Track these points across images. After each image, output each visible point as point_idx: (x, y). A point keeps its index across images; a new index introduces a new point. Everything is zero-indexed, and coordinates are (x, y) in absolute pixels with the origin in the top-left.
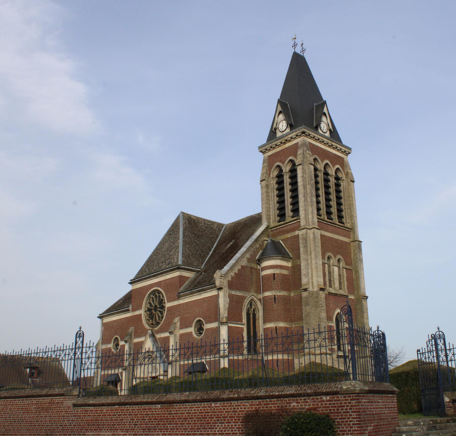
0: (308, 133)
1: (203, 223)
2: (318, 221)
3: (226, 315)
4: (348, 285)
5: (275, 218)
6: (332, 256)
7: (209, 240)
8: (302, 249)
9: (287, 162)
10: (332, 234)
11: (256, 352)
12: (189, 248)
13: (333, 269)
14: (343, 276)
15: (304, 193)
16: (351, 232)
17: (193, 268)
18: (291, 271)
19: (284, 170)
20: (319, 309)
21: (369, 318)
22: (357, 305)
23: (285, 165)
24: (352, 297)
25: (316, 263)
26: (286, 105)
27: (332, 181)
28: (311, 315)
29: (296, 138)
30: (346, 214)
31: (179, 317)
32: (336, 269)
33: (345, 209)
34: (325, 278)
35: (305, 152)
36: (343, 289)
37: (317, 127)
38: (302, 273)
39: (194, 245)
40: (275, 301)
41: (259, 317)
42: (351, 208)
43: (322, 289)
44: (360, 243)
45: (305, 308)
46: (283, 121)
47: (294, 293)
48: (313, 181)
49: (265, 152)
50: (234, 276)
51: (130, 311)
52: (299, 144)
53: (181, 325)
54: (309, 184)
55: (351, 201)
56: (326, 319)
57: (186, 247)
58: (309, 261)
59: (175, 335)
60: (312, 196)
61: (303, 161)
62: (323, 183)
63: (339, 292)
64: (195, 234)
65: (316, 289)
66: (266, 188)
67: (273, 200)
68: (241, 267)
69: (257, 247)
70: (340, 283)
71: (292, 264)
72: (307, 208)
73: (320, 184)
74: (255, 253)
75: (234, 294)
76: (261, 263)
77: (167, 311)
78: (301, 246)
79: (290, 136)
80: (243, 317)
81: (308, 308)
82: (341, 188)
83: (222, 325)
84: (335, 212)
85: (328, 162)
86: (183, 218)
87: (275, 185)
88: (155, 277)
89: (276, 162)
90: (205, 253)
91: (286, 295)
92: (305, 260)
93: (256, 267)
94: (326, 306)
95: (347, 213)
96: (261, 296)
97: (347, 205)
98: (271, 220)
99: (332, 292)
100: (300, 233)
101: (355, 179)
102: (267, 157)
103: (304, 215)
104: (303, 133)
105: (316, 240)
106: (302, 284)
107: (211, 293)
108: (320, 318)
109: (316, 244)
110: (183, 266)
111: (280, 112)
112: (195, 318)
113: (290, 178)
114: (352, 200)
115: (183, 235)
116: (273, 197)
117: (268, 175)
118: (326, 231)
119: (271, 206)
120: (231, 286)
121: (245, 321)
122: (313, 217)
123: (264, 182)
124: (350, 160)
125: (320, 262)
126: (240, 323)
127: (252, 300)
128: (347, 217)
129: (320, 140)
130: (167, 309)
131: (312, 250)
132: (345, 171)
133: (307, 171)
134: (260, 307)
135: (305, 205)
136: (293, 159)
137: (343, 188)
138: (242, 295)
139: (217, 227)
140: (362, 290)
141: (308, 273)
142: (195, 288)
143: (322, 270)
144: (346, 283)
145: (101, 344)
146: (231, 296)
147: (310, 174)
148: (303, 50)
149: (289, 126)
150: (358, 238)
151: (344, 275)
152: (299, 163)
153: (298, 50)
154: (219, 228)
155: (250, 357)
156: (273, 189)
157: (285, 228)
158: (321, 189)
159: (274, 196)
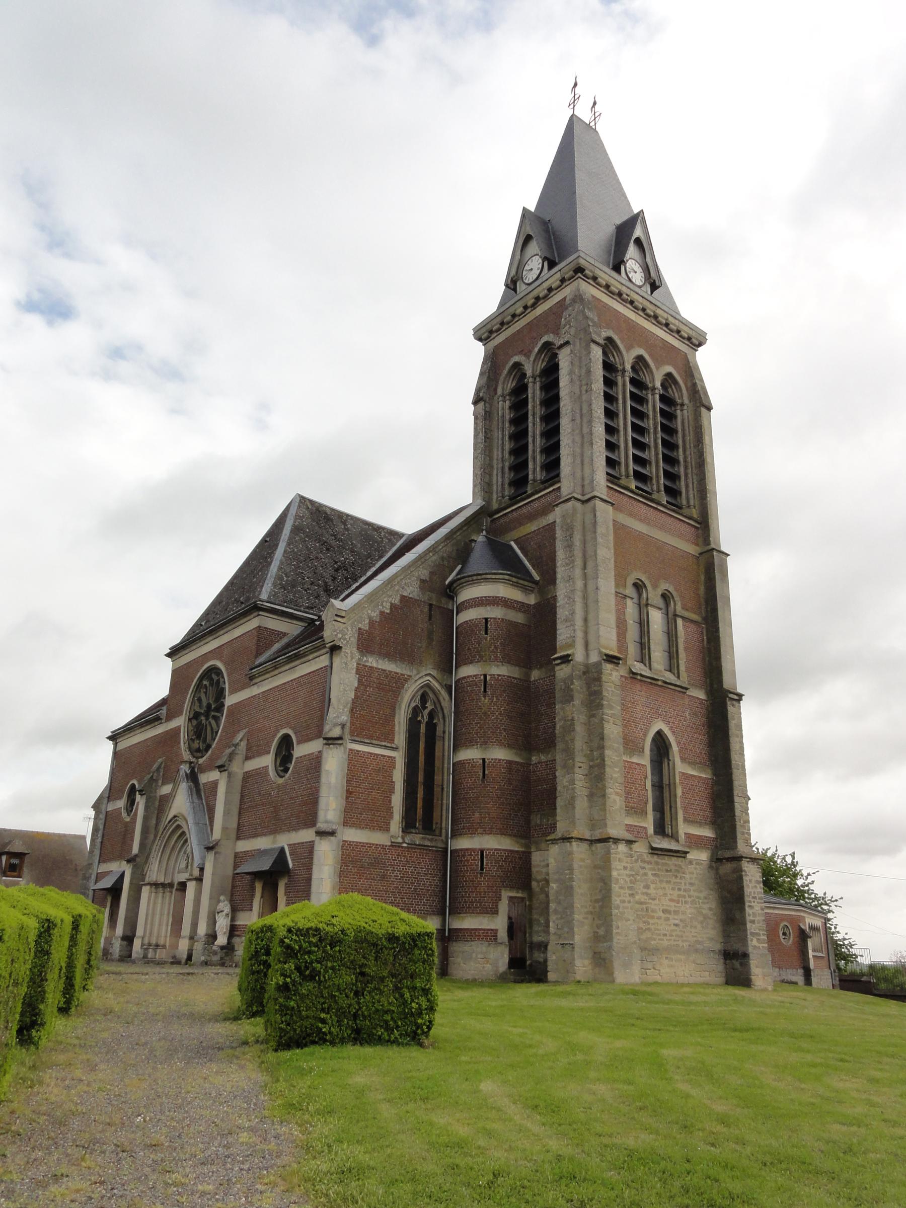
2: (608, 486)
8: (560, 555)
27: (654, 404)
38: (558, 616)
40: (485, 691)
41: (444, 732)
43: (612, 659)
51: (161, 719)
53: (249, 748)
68: (401, 601)
75: (375, 665)
83: (329, 744)
89: (512, 357)
91: (516, 676)
103: (570, 468)
106: (558, 644)
120: (366, 644)
121: (400, 737)
123: (481, 404)
124: (703, 358)
136: (550, 340)
138: (398, 670)
145: (105, 801)
146: (364, 674)
153: (584, 114)
157: (525, 510)
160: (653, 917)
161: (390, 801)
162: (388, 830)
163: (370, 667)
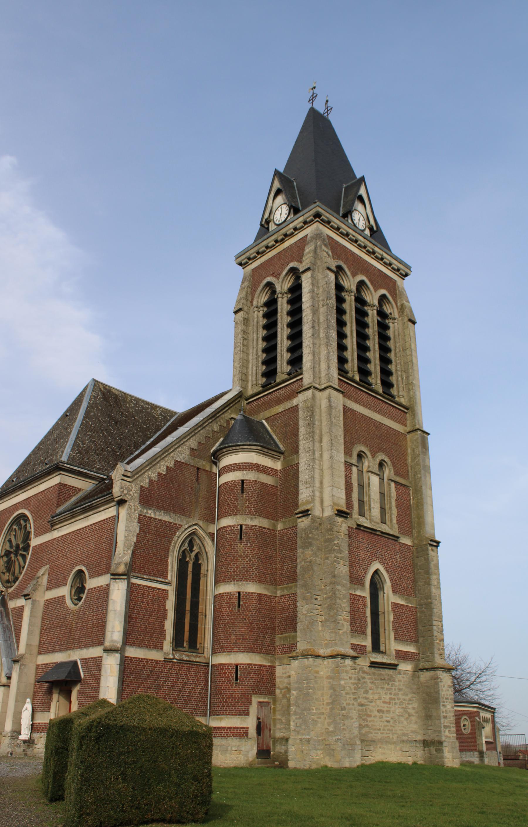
0: (326, 217)
1: (134, 404)
2: (339, 379)
3: (127, 558)
4: (399, 516)
5: (257, 380)
6: (368, 453)
7: (140, 431)
8: (302, 431)
9: (284, 273)
10: (369, 411)
11: (193, 644)
12: (91, 437)
13: (369, 479)
14: (390, 496)
15: (314, 321)
16: (407, 415)
17: (89, 472)
18: (281, 479)
19: (278, 289)
20: (333, 555)
21: (442, 586)
22: (417, 557)
23: (281, 279)
24: (406, 541)
25: (331, 458)
26: (291, 182)
27: (372, 318)
28: (315, 568)
29: (303, 227)
30: (397, 381)
31: (48, 566)
32: (375, 480)
33: (397, 370)
34: (351, 494)
35: (319, 249)
36: (388, 522)
37: (347, 214)
38: (300, 479)
39: (103, 434)
40: (241, 538)
41: (207, 571)
42: (408, 369)
43: (341, 513)
44: (425, 435)
45: (303, 553)
46: (283, 206)
47: (284, 522)
48: (333, 301)
49: (247, 263)
50: (155, 479)
52: (308, 237)
53: (49, 581)
54: (323, 306)
55: (408, 357)
56: (348, 578)
57: (86, 435)
58: (317, 454)
59: (34, 602)
60: (328, 327)
61: (314, 264)
62: (355, 340)
63: (380, 527)
64: (111, 418)
65: (328, 512)
66: (244, 324)
67: (255, 347)
68: (175, 464)
69: (215, 429)
70: (383, 509)
71: (283, 465)
72: (317, 351)
73: (348, 315)
74: (210, 440)
75: (153, 516)
76: (219, 460)
77: (31, 555)
78: (301, 423)
79: (292, 226)
80: (170, 568)
81: (308, 552)
82: (390, 333)
84: (376, 372)
85: (364, 278)
86: (94, 388)
87: (261, 319)
88: (23, 491)
89: (265, 278)
90: (125, 451)
91: (266, 526)
92: (308, 452)
93: (208, 469)
94: (351, 552)
95: (400, 379)
96: (213, 529)
97: (400, 363)
98: (250, 384)
99: (365, 525)
100: (299, 400)
101: (417, 319)
102: (249, 272)
104: (317, 215)
105: (333, 411)
106: (300, 501)
107: (105, 513)
108: (334, 576)
109: (333, 420)
110: (68, 466)
111: (278, 192)
112: (73, 567)
113: (289, 302)
114: (411, 355)
115: (85, 414)
116: (255, 340)
117: (249, 302)
118: (356, 401)
119: (251, 357)
121: (172, 575)
122: (329, 367)
123: (240, 314)
125: (341, 457)
126: (159, 579)
127: (194, 533)
128: (401, 385)
129: (350, 236)
130: (33, 550)
131: (323, 433)
132: (399, 304)
133: (322, 283)
134: (211, 549)
135: (314, 344)
136: (295, 266)
137: (394, 332)
138: (172, 521)
139: (161, 414)
140: (428, 528)
141: (313, 477)
142: (79, 504)
143: (343, 474)
144: (395, 511)
146: (142, 520)
147: (328, 287)
148: (328, 109)
149: (292, 211)
150: (422, 427)
151: (392, 495)
152: (306, 267)
153: (320, 108)
154: (165, 417)
155: (177, 656)
156: (258, 327)
157: (273, 395)
158: (348, 324)
159: (257, 340)
160: (370, 716)
161: (163, 626)
162: (161, 648)
163: (149, 517)
